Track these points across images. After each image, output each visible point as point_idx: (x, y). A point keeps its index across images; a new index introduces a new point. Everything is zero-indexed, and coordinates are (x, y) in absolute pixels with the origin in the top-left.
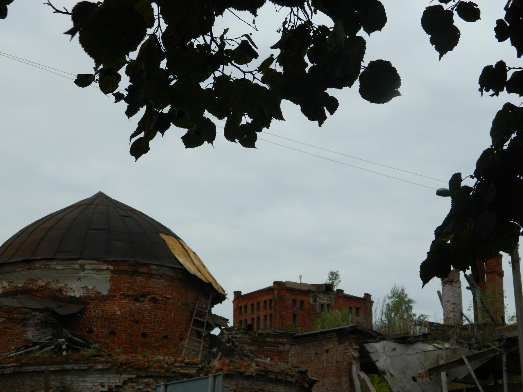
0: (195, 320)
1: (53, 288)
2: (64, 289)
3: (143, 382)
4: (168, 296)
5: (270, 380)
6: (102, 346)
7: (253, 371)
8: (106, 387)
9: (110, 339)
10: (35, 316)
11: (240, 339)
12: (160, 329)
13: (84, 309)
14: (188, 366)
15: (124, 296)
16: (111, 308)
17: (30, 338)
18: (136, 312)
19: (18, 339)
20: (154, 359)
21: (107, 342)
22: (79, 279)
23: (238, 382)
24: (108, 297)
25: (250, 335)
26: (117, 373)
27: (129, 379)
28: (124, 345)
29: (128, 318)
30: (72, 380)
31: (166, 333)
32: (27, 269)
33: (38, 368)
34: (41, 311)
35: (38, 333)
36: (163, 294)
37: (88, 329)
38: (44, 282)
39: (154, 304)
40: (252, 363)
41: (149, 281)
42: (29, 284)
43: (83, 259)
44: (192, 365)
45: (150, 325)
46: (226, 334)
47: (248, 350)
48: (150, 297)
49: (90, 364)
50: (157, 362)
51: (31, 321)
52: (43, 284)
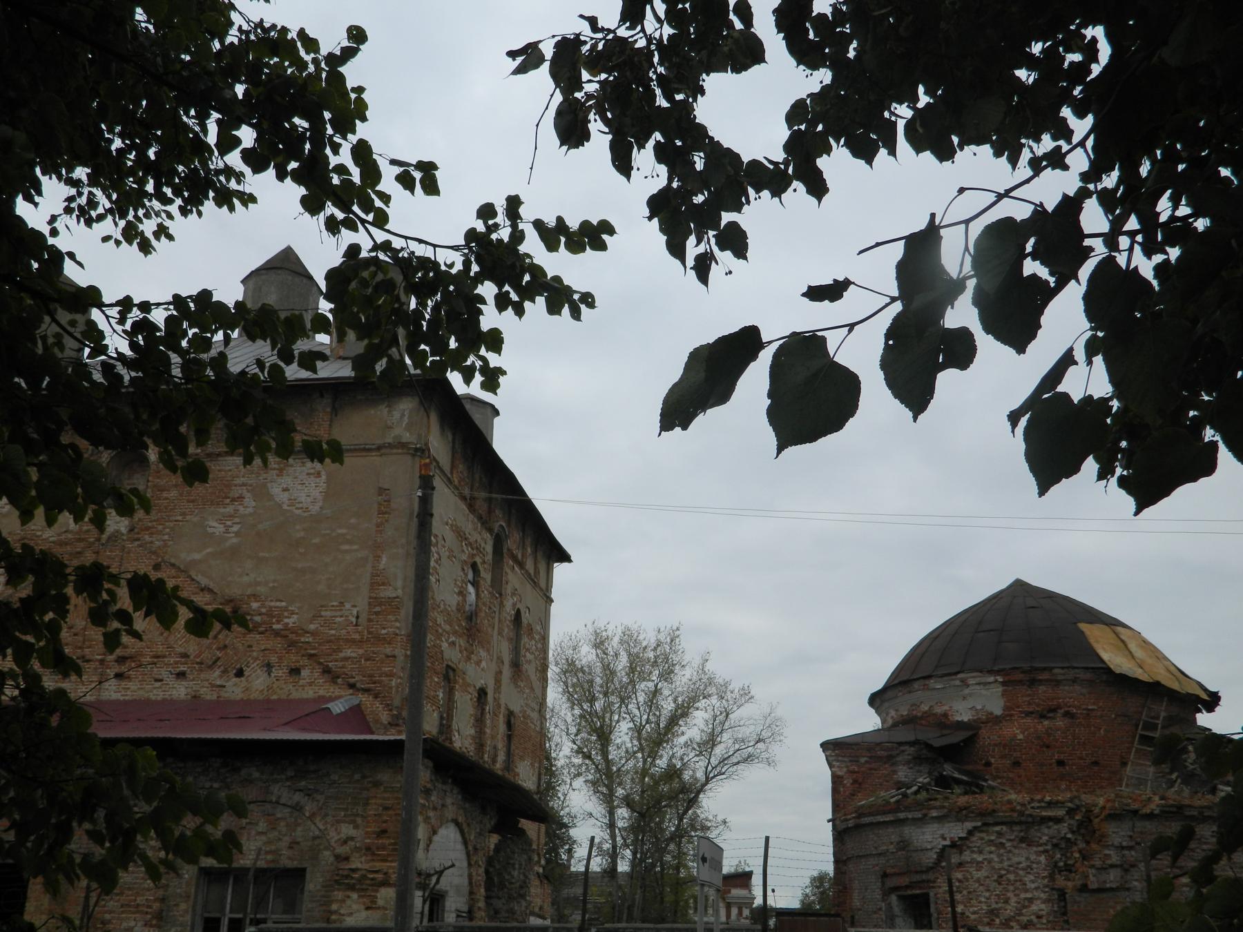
2: (950, 713)
3: (993, 832)
4: (1090, 707)
7: (1155, 808)
8: (948, 839)
10: (903, 751)
17: (903, 779)
19: (887, 781)
22: (964, 698)
23: (1134, 824)
39: (1070, 720)
42: (913, 710)
44: (1054, 804)
48: (1062, 711)
49: (924, 811)
52: (926, 709)
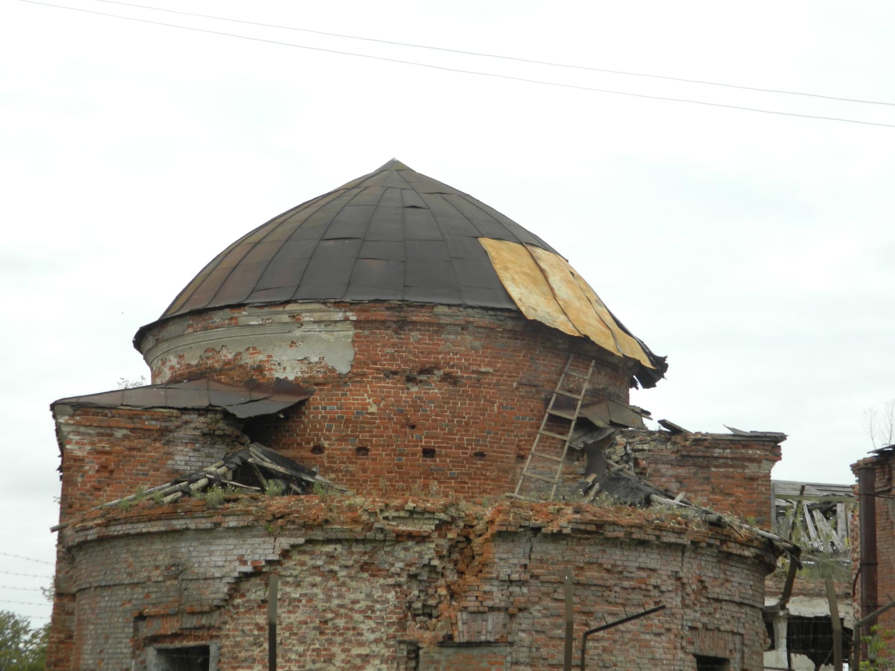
0: (550, 415)
1: (247, 364)
2: (267, 366)
4: (483, 369)
5: (615, 542)
6: (341, 477)
7: (565, 524)
8: (249, 563)
9: (357, 463)
10: (187, 422)
11: (651, 453)
12: (465, 438)
13: (302, 403)
14: (415, 516)
15: (385, 375)
16: (357, 400)
17: (181, 468)
18: (410, 406)
19: (157, 470)
20: (343, 503)
21: (351, 469)
24: (350, 378)
25: (675, 443)
26: (269, 535)
27: (294, 546)
28: (386, 474)
29: (393, 419)
30: (190, 551)
31: (478, 448)
32: (201, 330)
33: (133, 528)
34: (201, 411)
35: (198, 457)
36: (469, 364)
37: (312, 445)
38: (230, 353)
39: (451, 388)
40: (567, 507)
41: (438, 340)
42: (208, 358)
43: (295, 301)
45: (442, 432)
46: (620, 444)
47: (672, 476)
48: (442, 372)
49: (216, 519)
50: (349, 510)
51: (181, 433)
52: (230, 357)
